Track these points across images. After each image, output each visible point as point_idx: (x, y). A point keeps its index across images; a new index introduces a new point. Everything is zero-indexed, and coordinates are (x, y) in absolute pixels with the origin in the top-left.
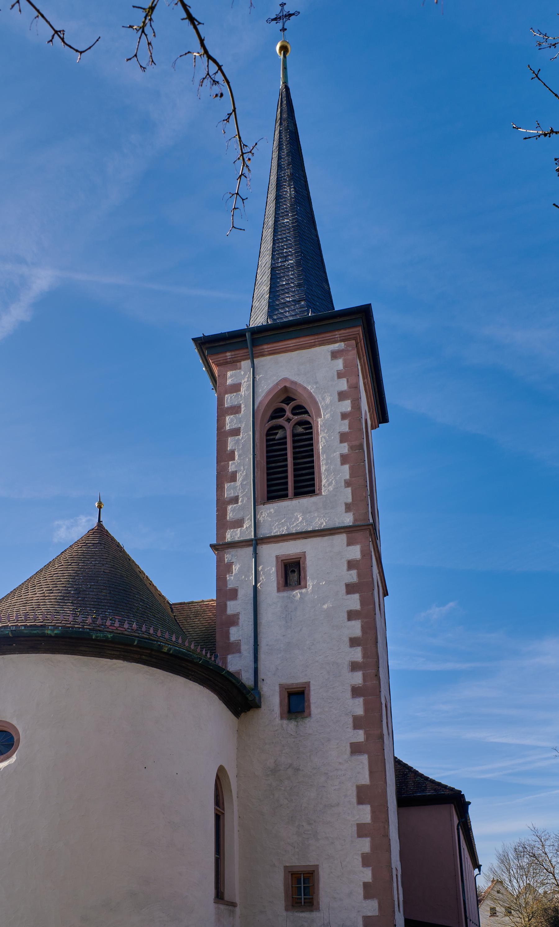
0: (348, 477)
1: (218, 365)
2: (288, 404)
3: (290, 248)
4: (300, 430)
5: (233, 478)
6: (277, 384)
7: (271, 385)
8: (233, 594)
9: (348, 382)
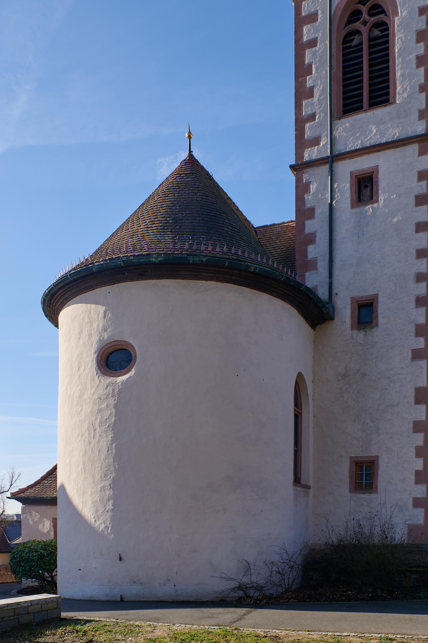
0: (422, 81)
5: (310, 94)
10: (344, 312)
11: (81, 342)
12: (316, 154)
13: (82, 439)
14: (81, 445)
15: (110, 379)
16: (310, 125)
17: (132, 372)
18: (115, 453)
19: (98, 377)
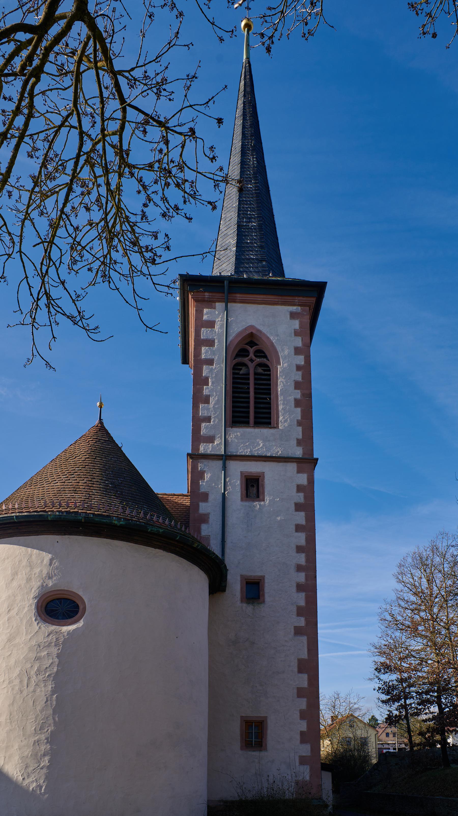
0: (299, 418)
1: (196, 300)
2: (252, 347)
3: (254, 211)
4: (260, 370)
5: (207, 400)
6: (246, 329)
7: (240, 329)
8: (205, 497)
9: (302, 340)
10: (235, 585)
11: (15, 584)
12: (210, 449)
13: (9, 686)
14: (8, 692)
15: (53, 628)
16: (205, 425)
17: (81, 624)
18: (56, 705)
19: (38, 624)
